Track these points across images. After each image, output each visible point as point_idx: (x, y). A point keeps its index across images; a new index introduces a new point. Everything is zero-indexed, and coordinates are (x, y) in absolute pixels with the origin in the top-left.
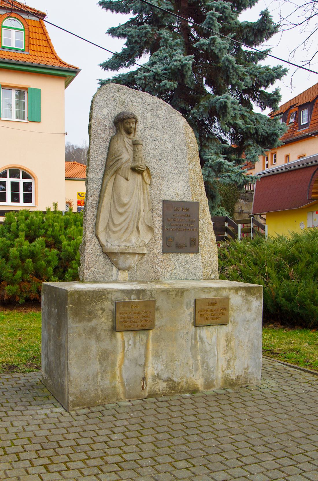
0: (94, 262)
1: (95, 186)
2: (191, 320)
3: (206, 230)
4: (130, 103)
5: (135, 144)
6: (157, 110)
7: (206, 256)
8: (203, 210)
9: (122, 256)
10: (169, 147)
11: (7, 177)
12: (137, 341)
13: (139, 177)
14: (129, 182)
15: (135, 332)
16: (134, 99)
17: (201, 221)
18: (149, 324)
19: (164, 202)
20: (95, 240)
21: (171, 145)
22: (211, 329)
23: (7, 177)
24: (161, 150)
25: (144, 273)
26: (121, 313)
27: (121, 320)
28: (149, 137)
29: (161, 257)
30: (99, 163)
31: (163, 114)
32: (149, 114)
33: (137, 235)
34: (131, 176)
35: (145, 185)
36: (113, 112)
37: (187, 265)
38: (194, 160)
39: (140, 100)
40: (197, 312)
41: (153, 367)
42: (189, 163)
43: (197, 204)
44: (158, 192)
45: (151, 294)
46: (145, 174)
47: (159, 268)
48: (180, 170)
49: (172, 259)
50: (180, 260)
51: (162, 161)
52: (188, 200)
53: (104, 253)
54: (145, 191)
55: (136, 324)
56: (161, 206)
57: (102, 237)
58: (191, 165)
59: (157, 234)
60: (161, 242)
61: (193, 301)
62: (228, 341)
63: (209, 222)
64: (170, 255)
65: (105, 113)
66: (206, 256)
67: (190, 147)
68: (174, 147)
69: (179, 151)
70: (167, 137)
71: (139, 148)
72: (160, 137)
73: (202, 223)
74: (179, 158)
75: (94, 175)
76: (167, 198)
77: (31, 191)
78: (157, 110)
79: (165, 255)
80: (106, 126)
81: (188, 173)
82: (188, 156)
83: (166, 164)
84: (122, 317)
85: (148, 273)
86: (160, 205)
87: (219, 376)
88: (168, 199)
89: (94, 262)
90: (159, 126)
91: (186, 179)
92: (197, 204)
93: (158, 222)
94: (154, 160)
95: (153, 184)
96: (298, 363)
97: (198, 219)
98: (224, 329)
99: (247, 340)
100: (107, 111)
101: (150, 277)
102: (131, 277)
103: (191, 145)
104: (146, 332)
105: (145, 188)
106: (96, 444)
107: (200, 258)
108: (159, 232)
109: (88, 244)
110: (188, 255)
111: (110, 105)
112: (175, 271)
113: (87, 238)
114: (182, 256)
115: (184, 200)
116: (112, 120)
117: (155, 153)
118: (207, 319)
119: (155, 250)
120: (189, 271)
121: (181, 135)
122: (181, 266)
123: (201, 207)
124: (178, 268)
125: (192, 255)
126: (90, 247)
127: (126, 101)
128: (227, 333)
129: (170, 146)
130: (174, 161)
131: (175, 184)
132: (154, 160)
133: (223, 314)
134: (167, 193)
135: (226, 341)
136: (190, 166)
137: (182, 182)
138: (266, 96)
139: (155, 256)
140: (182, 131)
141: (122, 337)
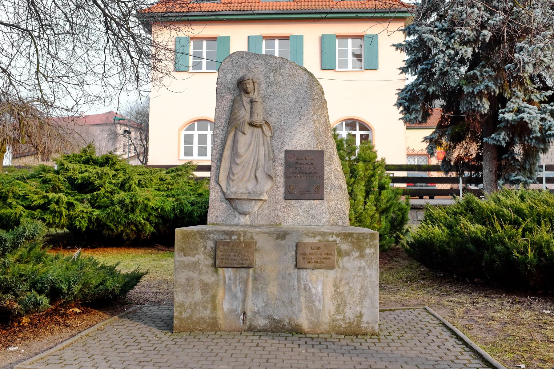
0: (217, 207)
1: (219, 141)
2: (293, 262)
3: (333, 178)
4: (253, 66)
5: (252, 102)
6: (280, 69)
7: (333, 203)
8: (330, 158)
10: (292, 101)
11: (194, 130)
13: (258, 131)
14: (247, 136)
15: (235, 269)
16: (257, 62)
17: (327, 169)
18: (248, 262)
19: (287, 152)
20: (217, 187)
21: (294, 99)
22: (316, 272)
23: (194, 130)
24: (284, 104)
25: (266, 218)
26: (221, 251)
27: (221, 257)
28: (271, 94)
29: (283, 203)
30: (223, 120)
31: (286, 72)
32: (272, 74)
33: (255, 183)
34: (248, 129)
35: (265, 137)
36: (237, 76)
37: (311, 212)
38: (319, 111)
39: (263, 62)
40: (298, 255)
41: (253, 304)
42: (314, 114)
43: (320, 154)
44: (280, 143)
45: (252, 236)
46: (265, 127)
47: (281, 214)
48: (304, 121)
49: (295, 205)
50: (304, 207)
51: (285, 114)
52: (312, 149)
53: (226, 199)
54: (266, 143)
55: (234, 262)
56: (283, 156)
57: (223, 184)
58: (316, 115)
59: (279, 182)
60: (283, 189)
61: (295, 244)
62: (336, 286)
65: (230, 78)
66: (333, 203)
67: (315, 99)
68: (297, 101)
69: (303, 104)
71: (255, 106)
72: (282, 92)
73: (328, 170)
74: (303, 110)
75: (218, 132)
77: (192, 144)
78: (280, 69)
79: (287, 201)
80: (230, 88)
81: (313, 123)
82: (313, 108)
83: (289, 117)
84: (221, 255)
85: (269, 218)
86: (283, 155)
87: (326, 319)
88: (291, 149)
89: (217, 207)
90: (282, 83)
91: (311, 129)
92: (320, 154)
93: (280, 170)
94: (276, 114)
95: (275, 136)
97: (322, 168)
99: (359, 287)
100: (231, 76)
101: (272, 222)
102: (252, 221)
104: (247, 270)
105: (265, 141)
107: (326, 204)
108: (281, 180)
109: (211, 192)
111: (234, 71)
112: (298, 217)
113: (211, 187)
114: (305, 203)
115: (309, 149)
116: (235, 83)
117: (277, 108)
119: (277, 197)
121: (305, 89)
122: (305, 212)
123: (327, 156)
124: (302, 214)
125: (316, 202)
126: (214, 194)
127: (249, 65)
130: (297, 114)
132: (276, 114)
133: (328, 258)
134: (290, 144)
135: (334, 286)
136: (315, 117)
137: (306, 133)
139: (277, 202)
140: (306, 85)
141: (223, 272)
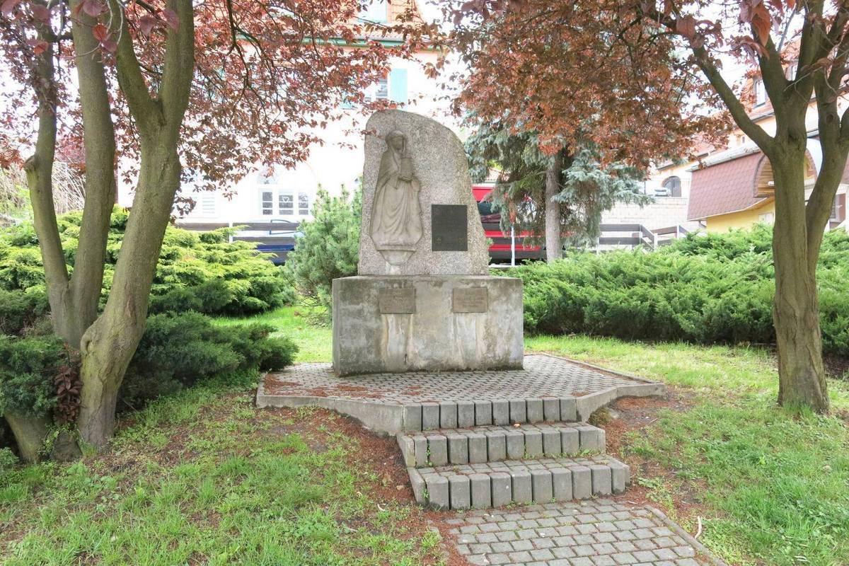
9: (393, 253)
12: (400, 322)
17: (470, 222)
19: (434, 206)
22: (470, 316)
29: (430, 254)
30: (373, 175)
43: (464, 208)
48: (448, 178)
63: (478, 223)
64: (439, 253)
68: (442, 158)
70: (435, 150)
76: (435, 203)
86: (430, 209)
92: (464, 208)
96: (203, 239)
98: (483, 317)
103: (459, 155)
106: (630, 550)
107: (469, 255)
110: (457, 252)
118: (464, 306)
120: (458, 267)
123: (470, 210)
125: (461, 253)
128: (487, 320)
129: (438, 157)
131: (443, 190)
133: (481, 303)
135: (486, 327)
136: (458, 174)
138: (138, 116)
139: (425, 253)
